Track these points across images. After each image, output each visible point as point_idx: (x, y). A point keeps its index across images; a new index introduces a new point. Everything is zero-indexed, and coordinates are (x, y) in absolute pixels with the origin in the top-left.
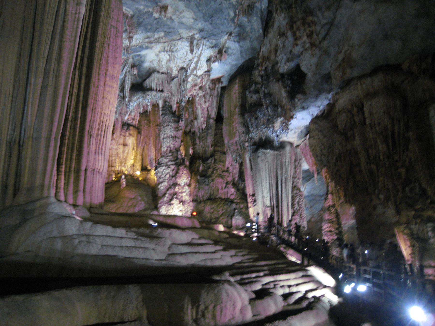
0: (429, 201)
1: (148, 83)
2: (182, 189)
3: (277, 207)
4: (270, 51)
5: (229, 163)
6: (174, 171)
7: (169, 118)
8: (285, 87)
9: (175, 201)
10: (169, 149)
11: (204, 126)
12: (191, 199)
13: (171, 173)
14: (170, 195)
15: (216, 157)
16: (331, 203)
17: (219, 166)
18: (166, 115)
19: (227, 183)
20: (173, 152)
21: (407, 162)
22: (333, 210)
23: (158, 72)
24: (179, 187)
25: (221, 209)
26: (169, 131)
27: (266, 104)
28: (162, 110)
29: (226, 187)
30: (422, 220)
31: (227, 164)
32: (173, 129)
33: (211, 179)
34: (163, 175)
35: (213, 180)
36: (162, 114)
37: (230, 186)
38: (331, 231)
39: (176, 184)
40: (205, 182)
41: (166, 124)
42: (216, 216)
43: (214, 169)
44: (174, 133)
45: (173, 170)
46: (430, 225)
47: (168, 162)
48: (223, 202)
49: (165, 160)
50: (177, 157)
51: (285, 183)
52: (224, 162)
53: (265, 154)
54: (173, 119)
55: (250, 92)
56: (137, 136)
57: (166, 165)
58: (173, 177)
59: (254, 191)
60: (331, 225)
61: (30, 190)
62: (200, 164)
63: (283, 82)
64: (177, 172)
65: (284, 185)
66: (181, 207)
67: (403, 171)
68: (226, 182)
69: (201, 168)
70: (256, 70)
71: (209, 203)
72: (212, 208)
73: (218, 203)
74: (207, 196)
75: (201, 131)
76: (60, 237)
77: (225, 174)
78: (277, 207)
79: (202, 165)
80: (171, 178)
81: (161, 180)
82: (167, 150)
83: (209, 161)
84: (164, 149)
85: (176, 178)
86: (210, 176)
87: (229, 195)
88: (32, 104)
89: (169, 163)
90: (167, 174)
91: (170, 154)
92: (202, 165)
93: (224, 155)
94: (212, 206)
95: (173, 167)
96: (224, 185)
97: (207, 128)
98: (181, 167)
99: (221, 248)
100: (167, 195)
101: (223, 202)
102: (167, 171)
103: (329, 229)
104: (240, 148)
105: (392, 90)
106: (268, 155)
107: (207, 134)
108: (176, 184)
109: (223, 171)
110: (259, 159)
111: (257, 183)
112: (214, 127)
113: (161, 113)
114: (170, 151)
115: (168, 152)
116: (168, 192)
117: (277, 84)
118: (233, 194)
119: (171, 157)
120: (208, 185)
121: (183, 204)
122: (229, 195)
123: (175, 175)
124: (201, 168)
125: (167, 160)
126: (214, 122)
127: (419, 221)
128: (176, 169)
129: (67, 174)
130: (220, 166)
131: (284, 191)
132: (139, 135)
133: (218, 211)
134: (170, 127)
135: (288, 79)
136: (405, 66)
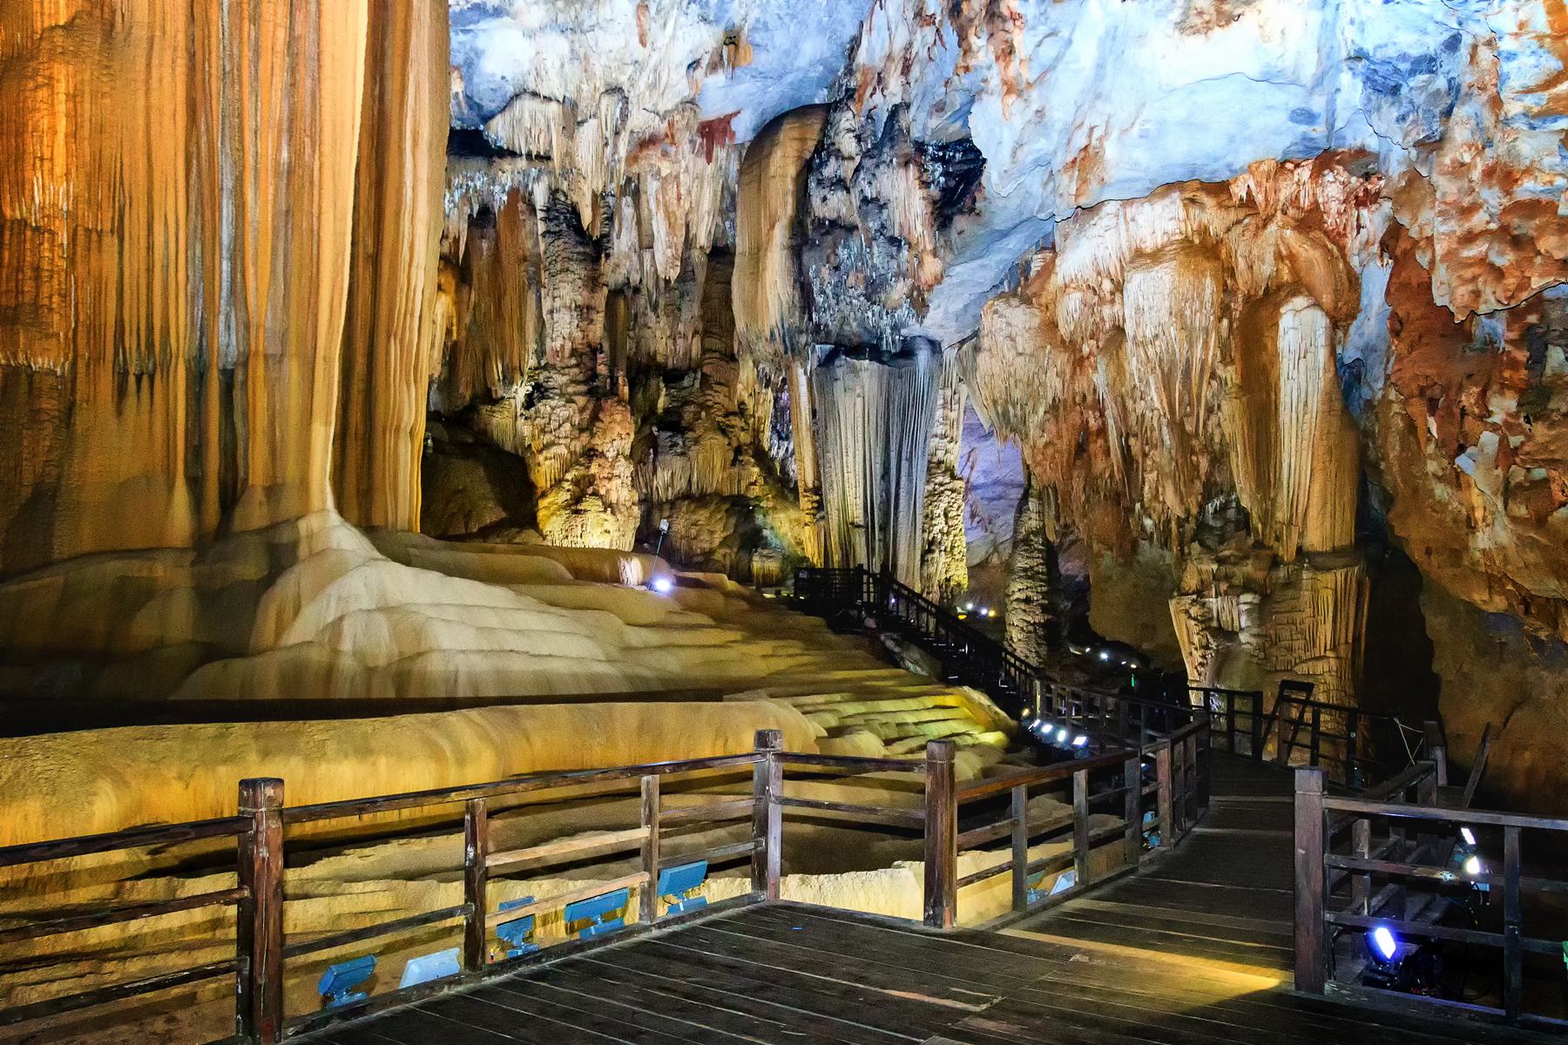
0: (1251, 541)
1: (499, 131)
2: (612, 467)
3: (884, 528)
4: (889, 57)
5: (746, 389)
6: (586, 415)
7: (565, 245)
8: (925, 184)
9: (591, 504)
10: (568, 346)
11: (674, 274)
12: (636, 498)
13: (576, 420)
14: (576, 482)
15: (705, 369)
16: (1034, 524)
17: (718, 397)
18: (558, 235)
19: (738, 451)
20: (581, 355)
21: (1217, 439)
22: (1037, 541)
23: (535, 94)
24: (602, 461)
25: (720, 526)
26: (569, 287)
27: (867, 230)
28: (545, 220)
29: (733, 464)
30: (1231, 586)
31: (742, 392)
32: (580, 283)
33: (690, 435)
34: (554, 425)
35: (696, 441)
36: (547, 233)
37: (748, 458)
38: (1028, 601)
39: (591, 454)
40: (676, 445)
41: (559, 267)
42: (706, 546)
43: (703, 406)
44: (585, 293)
45: (582, 410)
46: (1247, 597)
47: (567, 385)
48: (726, 506)
49: (559, 379)
50: (593, 369)
51: (910, 460)
52: (729, 384)
53: (855, 371)
54: (581, 249)
55: (820, 182)
56: (458, 290)
57: (561, 395)
58: (582, 430)
59: (818, 477)
60: (1029, 583)
61: (273, 490)
62: (659, 389)
63: (922, 169)
64: (595, 418)
65: (904, 464)
66: (610, 522)
67: (1204, 463)
68: (735, 444)
69: (661, 403)
70: (842, 110)
71: (685, 505)
72: (695, 524)
73: (713, 506)
74: (680, 485)
75: (662, 284)
76: (379, 609)
77: (737, 421)
78: (884, 528)
79: (664, 392)
80: (576, 433)
81: (548, 438)
82: (563, 346)
83: (686, 382)
84: (553, 344)
85: (592, 436)
86: (690, 428)
87: (744, 484)
88: (255, 264)
89: (570, 390)
90: (567, 419)
91: (573, 361)
92: (664, 392)
93: (732, 365)
94: (695, 517)
95: (581, 401)
96: (731, 455)
97: (686, 275)
98: (608, 404)
99: (738, 636)
100: (567, 485)
101: (726, 506)
102: (564, 413)
103: (1022, 596)
104: (782, 349)
105: (1203, 249)
106: (864, 375)
107: (682, 296)
108: (591, 454)
109: (728, 414)
110: (838, 387)
111: (830, 455)
112: (701, 275)
113: (541, 227)
114: (574, 353)
115: (567, 353)
116: (569, 476)
117: (902, 171)
118: (754, 484)
119: (576, 370)
120: (683, 454)
121: (613, 513)
122: (744, 484)
123: (590, 425)
124: (661, 403)
125: (565, 379)
126: (704, 259)
127: (1224, 587)
128: (591, 406)
129: (95, 330)
130: (720, 398)
131: (904, 480)
132: (465, 290)
133: (712, 533)
134: (571, 277)
135: (935, 159)
136: (1239, 191)
